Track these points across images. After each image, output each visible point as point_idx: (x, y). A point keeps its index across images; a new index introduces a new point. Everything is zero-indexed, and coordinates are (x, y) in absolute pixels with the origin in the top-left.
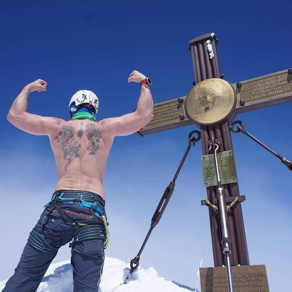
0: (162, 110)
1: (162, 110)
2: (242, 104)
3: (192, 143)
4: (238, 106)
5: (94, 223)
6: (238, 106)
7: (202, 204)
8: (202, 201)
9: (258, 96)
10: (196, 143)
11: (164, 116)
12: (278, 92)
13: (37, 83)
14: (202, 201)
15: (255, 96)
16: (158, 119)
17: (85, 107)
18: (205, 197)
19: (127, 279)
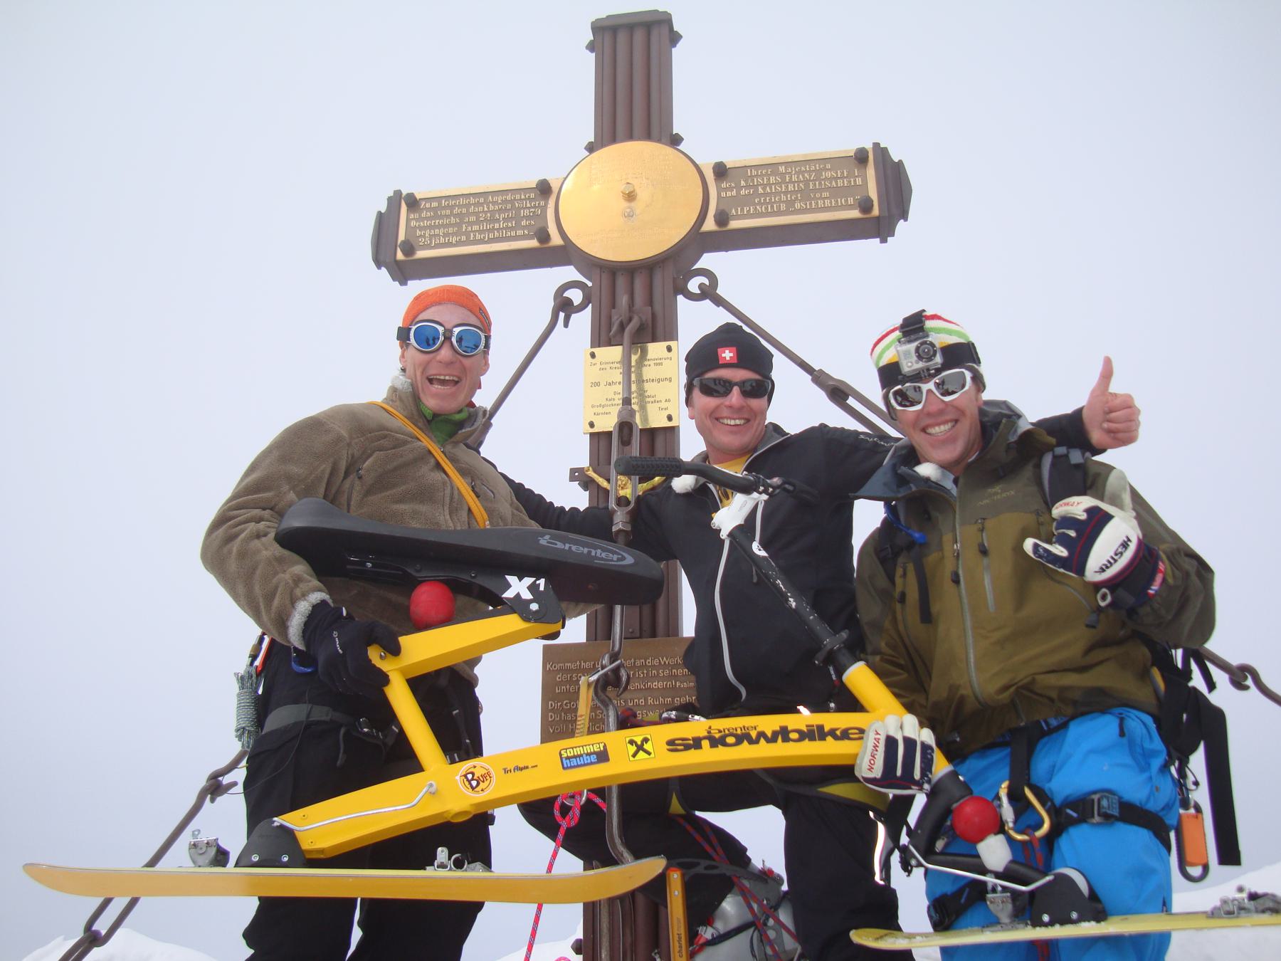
0: (481, 209)
1: (481, 209)
2: (722, 219)
3: (562, 315)
4: (710, 225)
5: (1221, 664)
6: (710, 225)
7: (572, 479)
8: (573, 471)
9: (767, 208)
10: (573, 316)
11: (485, 226)
12: (820, 203)
13: (785, 887)
14: (573, 471)
15: (758, 207)
16: (467, 234)
17: (517, 606)
18: (583, 461)
19: (32, 869)
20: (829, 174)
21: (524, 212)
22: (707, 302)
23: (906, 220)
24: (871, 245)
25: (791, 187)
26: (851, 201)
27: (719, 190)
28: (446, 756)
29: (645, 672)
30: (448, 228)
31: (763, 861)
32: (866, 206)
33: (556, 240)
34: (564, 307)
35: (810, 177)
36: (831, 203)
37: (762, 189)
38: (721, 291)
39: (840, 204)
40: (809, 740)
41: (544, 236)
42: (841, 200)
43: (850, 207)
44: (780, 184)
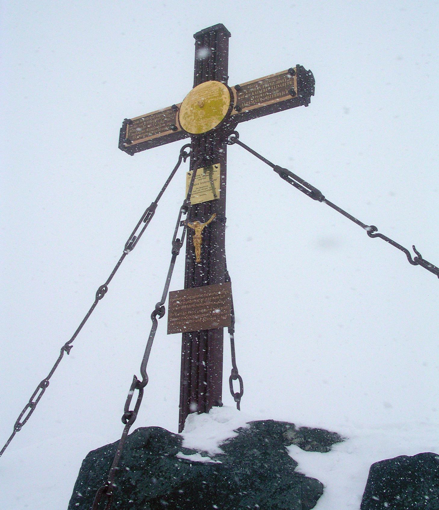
3: (183, 158)
20: (279, 82)
21: (266, 90)
22: (236, 145)
23: (313, 95)
24: (301, 109)
25: (264, 91)
26: (287, 92)
27: (238, 96)
28: (357, 220)
29: (180, 318)
30: (257, 96)
31: (238, 408)
32: (292, 92)
33: (180, 129)
34: (183, 155)
35: (282, 81)
36: (279, 94)
37: (254, 93)
38: (240, 139)
39: (180, 129)
40: (232, 369)
41: (175, 129)
42: (283, 92)
43: (286, 95)
44: (260, 90)
